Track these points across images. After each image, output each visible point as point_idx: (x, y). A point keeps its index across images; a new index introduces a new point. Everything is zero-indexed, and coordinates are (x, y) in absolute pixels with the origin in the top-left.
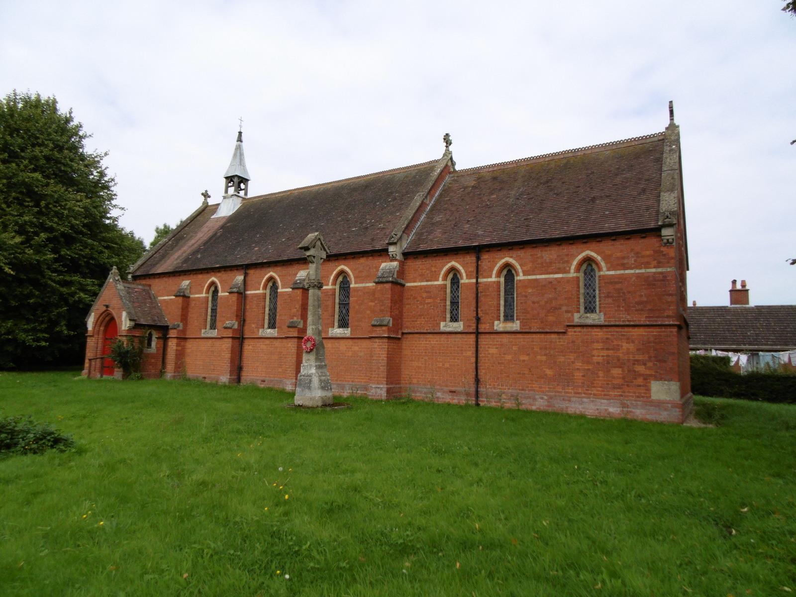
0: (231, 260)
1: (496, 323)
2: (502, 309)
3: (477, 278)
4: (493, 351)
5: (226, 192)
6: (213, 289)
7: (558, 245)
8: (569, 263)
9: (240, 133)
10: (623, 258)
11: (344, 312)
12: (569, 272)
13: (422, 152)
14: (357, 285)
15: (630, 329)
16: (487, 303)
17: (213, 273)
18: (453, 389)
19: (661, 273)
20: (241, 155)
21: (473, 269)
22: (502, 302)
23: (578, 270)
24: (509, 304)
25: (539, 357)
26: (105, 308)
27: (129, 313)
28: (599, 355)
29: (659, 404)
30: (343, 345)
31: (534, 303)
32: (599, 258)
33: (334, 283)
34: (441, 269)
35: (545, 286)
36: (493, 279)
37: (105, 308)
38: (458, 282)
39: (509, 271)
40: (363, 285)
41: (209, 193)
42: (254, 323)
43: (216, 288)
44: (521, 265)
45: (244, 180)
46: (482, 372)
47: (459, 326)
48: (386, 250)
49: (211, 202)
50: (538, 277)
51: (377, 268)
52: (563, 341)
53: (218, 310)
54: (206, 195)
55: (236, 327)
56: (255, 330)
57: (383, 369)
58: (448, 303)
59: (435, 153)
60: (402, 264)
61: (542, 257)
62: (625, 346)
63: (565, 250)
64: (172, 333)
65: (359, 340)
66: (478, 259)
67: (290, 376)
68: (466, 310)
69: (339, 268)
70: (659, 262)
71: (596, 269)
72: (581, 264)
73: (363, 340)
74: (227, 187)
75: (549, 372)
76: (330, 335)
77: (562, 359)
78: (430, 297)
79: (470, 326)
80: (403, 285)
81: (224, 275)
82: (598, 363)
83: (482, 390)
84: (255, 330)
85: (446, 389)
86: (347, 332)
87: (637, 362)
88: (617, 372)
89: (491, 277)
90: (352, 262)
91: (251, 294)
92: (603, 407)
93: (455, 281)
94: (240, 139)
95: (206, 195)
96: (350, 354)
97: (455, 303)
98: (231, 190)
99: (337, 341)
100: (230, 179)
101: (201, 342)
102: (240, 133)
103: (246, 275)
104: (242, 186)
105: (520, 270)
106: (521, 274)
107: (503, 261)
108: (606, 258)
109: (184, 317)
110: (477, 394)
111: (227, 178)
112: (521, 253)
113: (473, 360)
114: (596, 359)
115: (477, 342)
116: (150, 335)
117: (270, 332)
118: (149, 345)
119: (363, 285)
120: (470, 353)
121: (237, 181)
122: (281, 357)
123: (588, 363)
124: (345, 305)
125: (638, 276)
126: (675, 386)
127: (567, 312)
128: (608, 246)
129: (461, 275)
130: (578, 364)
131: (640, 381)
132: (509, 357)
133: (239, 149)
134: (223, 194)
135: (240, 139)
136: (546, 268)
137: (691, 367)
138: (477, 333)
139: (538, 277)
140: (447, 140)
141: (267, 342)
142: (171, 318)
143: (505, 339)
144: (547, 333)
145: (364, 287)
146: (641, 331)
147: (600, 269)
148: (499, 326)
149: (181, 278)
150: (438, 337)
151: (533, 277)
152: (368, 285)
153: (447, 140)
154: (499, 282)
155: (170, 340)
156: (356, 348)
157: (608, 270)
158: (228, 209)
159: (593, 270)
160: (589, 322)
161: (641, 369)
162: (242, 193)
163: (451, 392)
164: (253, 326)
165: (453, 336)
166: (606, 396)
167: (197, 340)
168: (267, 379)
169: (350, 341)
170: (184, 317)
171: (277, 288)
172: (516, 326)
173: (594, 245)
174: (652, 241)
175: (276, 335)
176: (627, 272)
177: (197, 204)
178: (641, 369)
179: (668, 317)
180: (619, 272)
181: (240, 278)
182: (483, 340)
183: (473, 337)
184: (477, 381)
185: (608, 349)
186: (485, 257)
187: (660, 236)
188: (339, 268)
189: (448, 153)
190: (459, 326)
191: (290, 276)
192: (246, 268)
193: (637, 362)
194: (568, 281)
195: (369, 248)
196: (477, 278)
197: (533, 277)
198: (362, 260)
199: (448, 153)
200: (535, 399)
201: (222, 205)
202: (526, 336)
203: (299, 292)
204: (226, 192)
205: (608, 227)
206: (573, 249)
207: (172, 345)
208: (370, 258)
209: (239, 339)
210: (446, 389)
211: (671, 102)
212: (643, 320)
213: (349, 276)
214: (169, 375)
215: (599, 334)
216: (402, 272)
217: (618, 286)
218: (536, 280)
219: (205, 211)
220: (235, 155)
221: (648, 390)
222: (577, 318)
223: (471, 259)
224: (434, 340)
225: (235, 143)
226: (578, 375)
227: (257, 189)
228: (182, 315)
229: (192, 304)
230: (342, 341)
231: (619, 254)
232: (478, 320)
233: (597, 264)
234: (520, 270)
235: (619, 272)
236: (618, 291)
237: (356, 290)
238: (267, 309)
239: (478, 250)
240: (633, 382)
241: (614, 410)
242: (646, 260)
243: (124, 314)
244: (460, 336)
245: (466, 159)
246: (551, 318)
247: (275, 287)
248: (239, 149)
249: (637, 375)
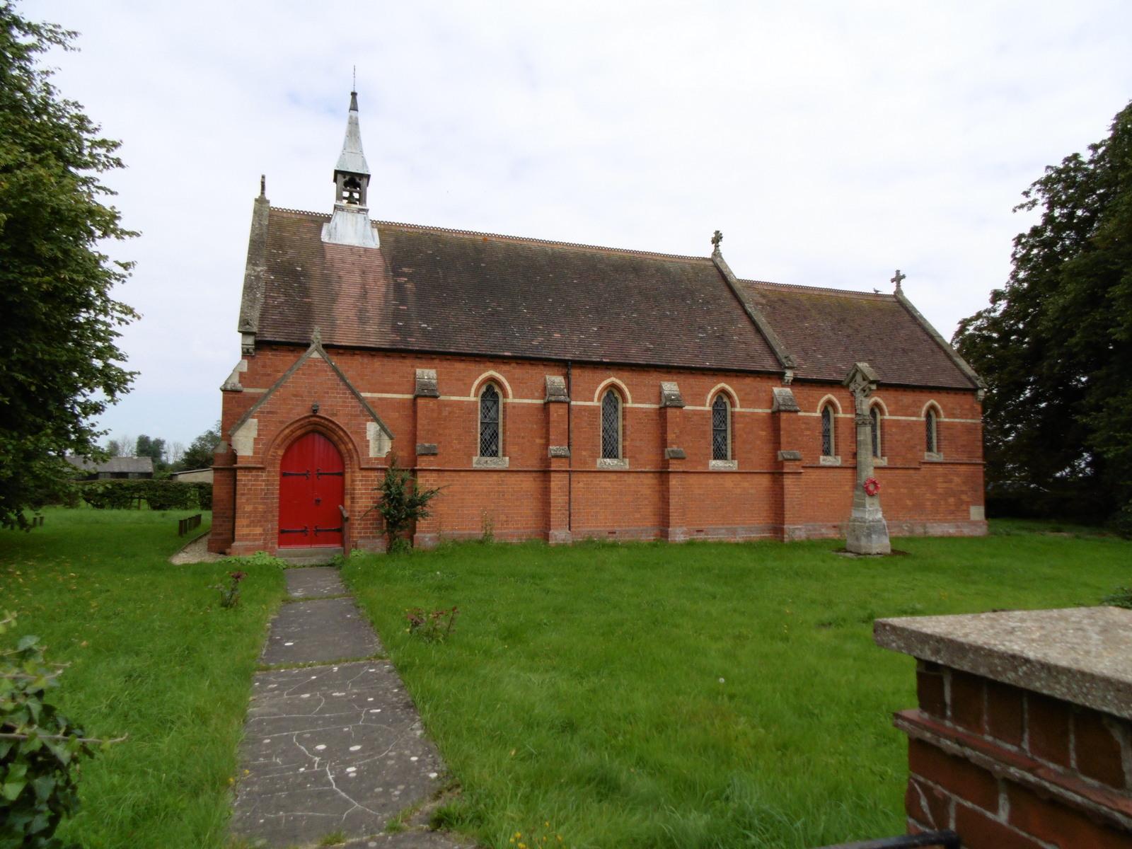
0: (536, 344)
2: (501, 430)
7: (544, 365)
9: (354, 94)
11: (719, 440)
14: (743, 410)
15: (958, 466)
17: (491, 364)
18: (700, 528)
25: (902, 490)
28: (941, 487)
29: (975, 523)
30: (728, 482)
31: (897, 441)
33: (476, 395)
34: (819, 400)
35: (904, 426)
40: (751, 410)
41: (894, 276)
42: (585, 450)
44: (887, 406)
50: (900, 418)
56: (589, 460)
59: (706, 251)
61: (902, 400)
65: (749, 476)
67: (677, 523)
69: (720, 386)
70: (974, 415)
71: (620, 400)
73: (754, 475)
75: (909, 503)
76: (711, 469)
78: (807, 429)
79: (846, 461)
82: (940, 494)
84: (589, 460)
85: (829, 524)
86: (733, 465)
87: (963, 492)
88: (951, 500)
89: (593, 401)
90: (735, 381)
91: (576, 406)
92: (946, 530)
94: (354, 107)
96: (738, 491)
99: (722, 475)
101: (471, 477)
102: (354, 94)
103: (567, 377)
108: (944, 407)
114: (940, 491)
117: (610, 463)
119: (751, 410)
122: (638, 498)
124: (719, 431)
125: (962, 424)
127: (920, 450)
128: (950, 400)
130: (928, 496)
131: (964, 507)
135: (354, 107)
139: (900, 418)
141: (613, 477)
144: (908, 468)
145: (753, 413)
146: (963, 468)
147: (625, 400)
150: (818, 472)
152: (756, 410)
155: (671, 476)
156: (746, 485)
157: (945, 417)
161: (964, 497)
163: (834, 527)
164: (584, 453)
165: (832, 470)
166: (946, 521)
167: (462, 474)
168: (616, 529)
169: (737, 475)
173: (626, 374)
174: (969, 398)
175: (627, 467)
178: (964, 497)
181: (556, 380)
182: (566, 475)
185: (946, 482)
188: (720, 386)
189: (717, 254)
190: (838, 461)
191: (645, 386)
192: (565, 366)
193: (963, 492)
198: (748, 381)
202: (893, 471)
208: (759, 379)
210: (829, 524)
211: (263, 177)
215: (940, 469)
218: (898, 420)
221: (968, 511)
224: (814, 475)
230: (728, 476)
240: (959, 511)
241: (952, 531)
245: (744, 266)
246: (909, 456)
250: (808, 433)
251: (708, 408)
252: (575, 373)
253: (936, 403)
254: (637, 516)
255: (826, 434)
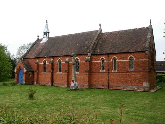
1: (112, 70)
2: (113, 67)
3: (108, 61)
4: (112, 77)
5: (44, 36)
6: (44, 62)
8: (127, 58)
9: (47, 20)
10: (138, 57)
12: (127, 60)
13: (96, 28)
16: (111, 66)
19: (145, 60)
20: (47, 26)
21: (107, 58)
22: (113, 66)
23: (129, 59)
24: (115, 66)
26: (19, 67)
27: (25, 68)
28: (133, 77)
32: (105, 59)
36: (112, 61)
37: (19, 67)
38: (104, 61)
39: (115, 59)
40: (82, 62)
43: (45, 62)
45: (49, 33)
46: (109, 81)
47: (104, 71)
48: (87, 54)
49: (40, 38)
51: (85, 58)
52: (127, 74)
53: (47, 67)
54: (38, 36)
55: (51, 71)
57: (88, 81)
58: (102, 66)
59: (97, 28)
60: (91, 57)
62: (139, 75)
63: (127, 55)
64: (36, 73)
66: (108, 56)
68: (106, 68)
72: (130, 58)
74: (44, 35)
75: (123, 81)
77: (126, 78)
80: (91, 62)
81: (47, 59)
83: (109, 85)
86: (79, 72)
88: (137, 81)
93: (103, 61)
94: (47, 22)
95: (38, 36)
97: (103, 66)
98: (45, 35)
100: (44, 33)
103: (53, 59)
104: (48, 34)
105: (117, 59)
106: (117, 60)
107: (130, 56)
109: (38, 69)
110: (108, 86)
111: (44, 32)
112: (117, 55)
113: (107, 78)
115: (108, 75)
116: (30, 73)
118: (30, 76)
119: (82, 62)
120: (107, 77)
121: (47, 33)
123: (131, 79)
125: (141, 61)
126: (148, 83)
128: (137, 55)
129: (104, 60)
130: (129, 79)
131: (141, 83)
132: (115, 78)
133: (47, 25)
134: (43, 36)
135: (47, 22)
136: (123, 59)
137: (26, 84)
138: (108, 73)
140: (100, 26)
142: (35, 68)
143: (114, 74)
146: (142, 72)
147: (134, 59)
148: (113, 71)
149: (36, 59)
151: (120, 61)
153: (100, 26)
154: (113, 62)
158: (45, 40)
159: (132, 59)
160: (132, 70)
161: (142, 80)
162: (48, 36)
170: (38, 69)
171: (61, 62)
172: (117, 71)
175: (61, 73)
176: (139, 60)
177: (36, 38)
178: (142, 80)
179: (147, 69)
180: (137, 60)
182: (110, 74)
183: (107, 73)
184: (108, 83)
186: (110, 56)
187: (145, 53)
189: (100, 28)
190: (104, 71)
194: (127, 62)
195: (83, 53)
196: (108, 61)
197: (120, 61)
198: (82, 56)
199: (100, 28)
200: (120, 87)
201: (43, 39)
203: (37, 65)
204: (44, 36)
205: (135, 50)
206: (128, 55)
207: (36, 76)
209: (52, 74)
211: (150, 20)
212: (142, 70)
213: (79, 60)
214: (35, 83)
215: (133, 73)
216: (91, 59)
217: (137, 63)
219: (38, 41)
220: (46, 26)
221: (143, 84)
222: (129, 70)
223: (106, 56)
224: (99, 74)
225: (45, 23)
226: (129, 81)
227: (51, 36)
228: (38, 68)
229: (54, 65)
231: (138, 56)
232: (108, 70)
233: (133, 58)
234: (117, 59)
235: (137, 60)
236: (137, 64)
237: (80, 63)
238: (59, 67)
239: (108, 54)
242: (143, 57)
243: (24, 68)
244: (104, 73)
245: (105, 30)
247: (45, 63)
248: (47, 25)
249: (141, 81)
250: (97, 65)
251: (128, 60)
252: (54, 58)
253: (115, 57)
254: (63, 81)
255: (45, 67)
